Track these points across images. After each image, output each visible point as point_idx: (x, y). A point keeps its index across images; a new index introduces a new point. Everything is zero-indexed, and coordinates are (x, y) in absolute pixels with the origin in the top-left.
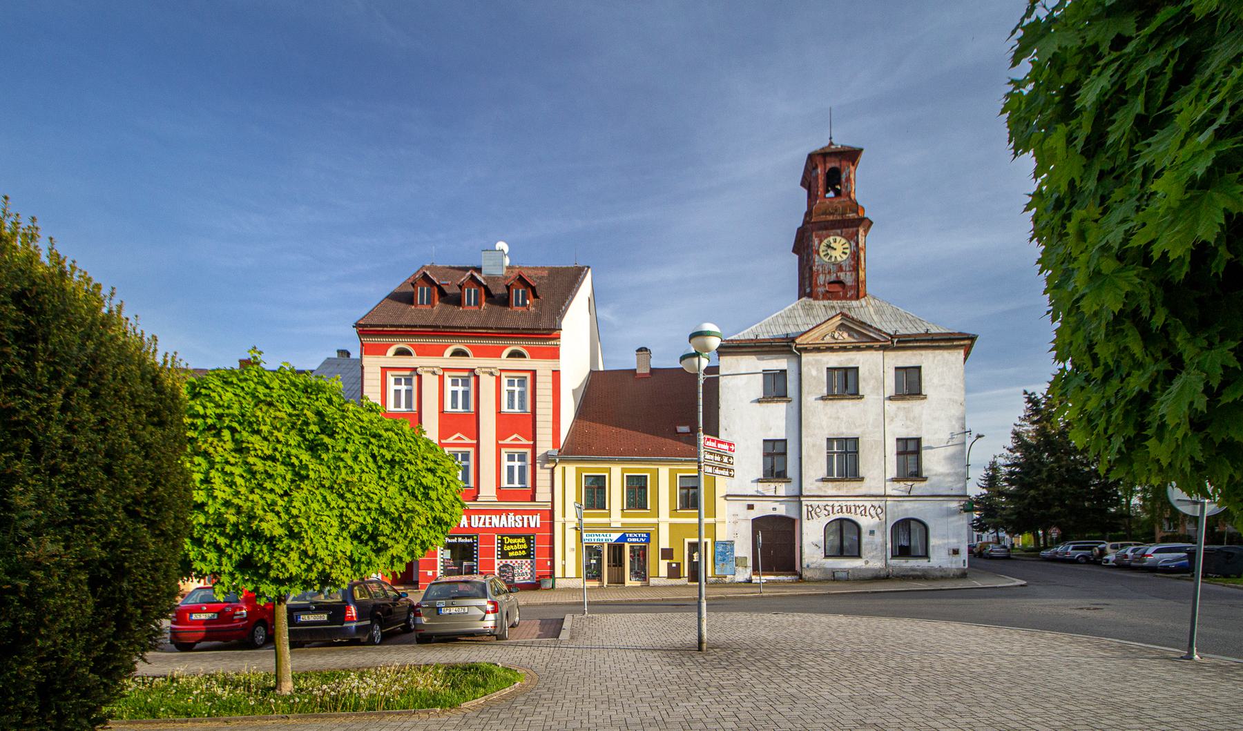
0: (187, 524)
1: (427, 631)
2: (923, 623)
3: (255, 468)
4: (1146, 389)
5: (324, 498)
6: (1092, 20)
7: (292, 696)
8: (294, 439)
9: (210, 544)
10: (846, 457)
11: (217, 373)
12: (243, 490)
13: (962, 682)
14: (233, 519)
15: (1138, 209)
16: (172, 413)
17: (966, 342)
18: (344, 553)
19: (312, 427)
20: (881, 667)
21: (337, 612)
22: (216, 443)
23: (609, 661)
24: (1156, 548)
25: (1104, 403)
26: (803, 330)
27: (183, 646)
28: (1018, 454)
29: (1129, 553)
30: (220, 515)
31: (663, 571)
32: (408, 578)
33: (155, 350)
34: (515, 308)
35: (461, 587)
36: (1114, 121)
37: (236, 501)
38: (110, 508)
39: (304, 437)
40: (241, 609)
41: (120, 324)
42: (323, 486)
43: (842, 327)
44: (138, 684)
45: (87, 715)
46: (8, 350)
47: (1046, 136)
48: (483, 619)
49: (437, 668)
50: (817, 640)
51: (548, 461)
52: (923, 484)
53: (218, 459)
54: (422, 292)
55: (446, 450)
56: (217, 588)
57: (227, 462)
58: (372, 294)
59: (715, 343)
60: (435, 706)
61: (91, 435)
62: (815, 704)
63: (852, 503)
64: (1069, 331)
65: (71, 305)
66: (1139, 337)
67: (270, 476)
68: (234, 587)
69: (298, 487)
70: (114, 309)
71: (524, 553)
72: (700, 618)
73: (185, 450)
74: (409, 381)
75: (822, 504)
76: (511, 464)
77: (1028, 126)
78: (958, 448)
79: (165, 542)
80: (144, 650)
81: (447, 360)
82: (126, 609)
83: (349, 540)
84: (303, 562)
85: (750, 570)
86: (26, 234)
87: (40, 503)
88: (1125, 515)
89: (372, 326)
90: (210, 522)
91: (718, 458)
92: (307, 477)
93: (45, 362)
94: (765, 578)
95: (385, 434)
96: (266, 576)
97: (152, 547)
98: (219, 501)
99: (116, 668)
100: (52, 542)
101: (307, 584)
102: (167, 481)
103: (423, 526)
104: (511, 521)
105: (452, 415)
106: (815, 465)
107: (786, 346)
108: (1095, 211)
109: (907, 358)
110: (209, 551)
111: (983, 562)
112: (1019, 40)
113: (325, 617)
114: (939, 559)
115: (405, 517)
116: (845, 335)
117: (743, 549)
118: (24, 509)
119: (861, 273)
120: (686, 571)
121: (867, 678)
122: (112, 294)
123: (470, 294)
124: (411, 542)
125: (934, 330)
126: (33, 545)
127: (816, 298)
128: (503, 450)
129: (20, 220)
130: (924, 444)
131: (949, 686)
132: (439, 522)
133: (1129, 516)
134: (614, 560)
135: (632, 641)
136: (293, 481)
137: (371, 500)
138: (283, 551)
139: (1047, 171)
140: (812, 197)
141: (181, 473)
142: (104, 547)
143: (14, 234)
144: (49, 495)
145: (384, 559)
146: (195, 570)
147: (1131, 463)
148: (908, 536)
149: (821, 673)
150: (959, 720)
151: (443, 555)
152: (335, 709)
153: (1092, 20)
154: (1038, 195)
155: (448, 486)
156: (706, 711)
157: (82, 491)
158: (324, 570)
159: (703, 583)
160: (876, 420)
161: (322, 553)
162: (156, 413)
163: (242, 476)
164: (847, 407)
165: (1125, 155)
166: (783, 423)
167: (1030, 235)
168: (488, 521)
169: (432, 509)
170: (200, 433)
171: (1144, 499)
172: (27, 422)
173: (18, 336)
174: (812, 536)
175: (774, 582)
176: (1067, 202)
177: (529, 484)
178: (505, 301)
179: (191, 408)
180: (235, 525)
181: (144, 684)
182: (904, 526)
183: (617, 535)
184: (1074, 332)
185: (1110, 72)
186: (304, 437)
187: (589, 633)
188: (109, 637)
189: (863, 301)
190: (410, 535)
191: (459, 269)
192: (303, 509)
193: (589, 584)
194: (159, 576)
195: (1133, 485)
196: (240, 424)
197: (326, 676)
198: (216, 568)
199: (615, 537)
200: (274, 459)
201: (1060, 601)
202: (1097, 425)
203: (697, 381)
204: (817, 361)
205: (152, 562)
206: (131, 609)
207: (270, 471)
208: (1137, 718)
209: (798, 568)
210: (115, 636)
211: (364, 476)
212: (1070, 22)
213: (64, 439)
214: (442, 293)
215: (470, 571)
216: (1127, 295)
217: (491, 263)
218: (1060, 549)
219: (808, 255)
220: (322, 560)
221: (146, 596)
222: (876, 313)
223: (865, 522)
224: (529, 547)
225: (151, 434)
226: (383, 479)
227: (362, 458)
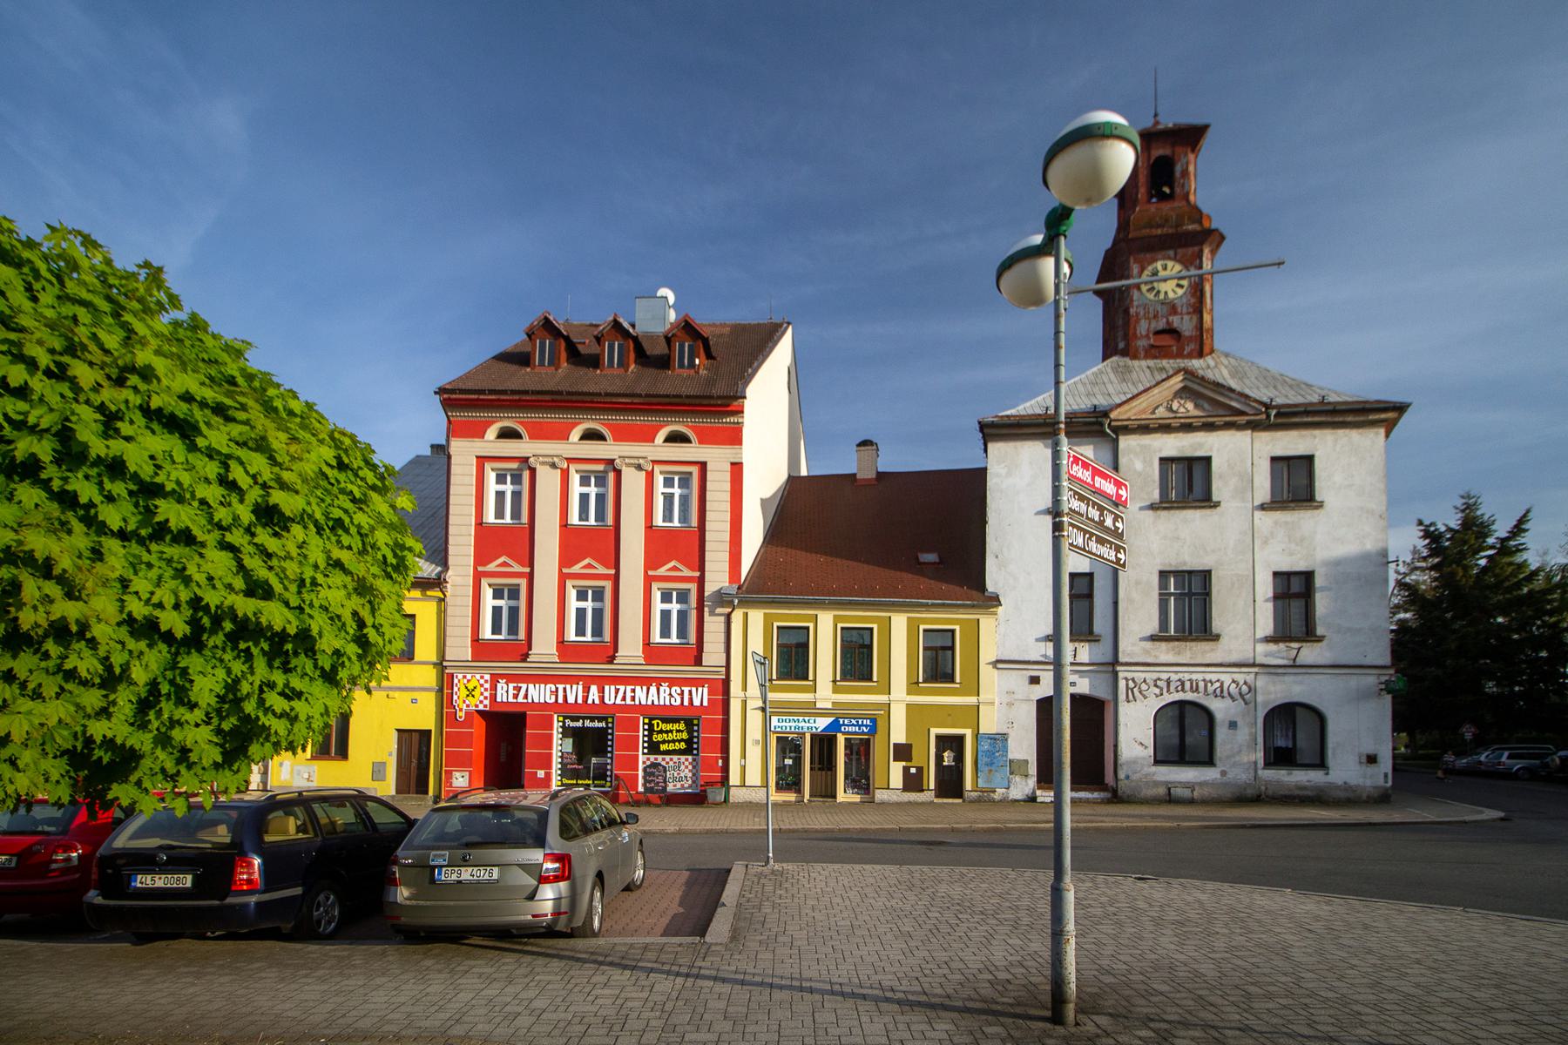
10: (1190, 601)
17: (1390, 415)
21: (215, 869)
26: (1118, 401)
28: (1408, 615)
34: (678, 371)
43: (1184, 392)
51: (722, 603)
63: (1200, 677)
71: (683, 745)
75: (1150, 677)
76: (666, 606)
81: (573, 445)
85: (1032, 782)
91: (1094, 514)
104: (665, 696)
105: (578, 530)
106: (1139, 613)
107: (1095, 425)
109: (1291, 443)
113: (187, 881)
114: (1344, 769)
116: (1190, 406)
117: (1023, 747)
119: (1207, 317)
120: (931, 781)
123: (613, 350)
125: (1333, 398)
127: (1135, 357)
128: (655, 586)
134: (812, 761)
148: (1292, 732)
164: (1192, 521)
168: (629, 694)
174: (1134, 732)
177: (693, 639)
182: (1284, 715)
189: (1209, 360)
199: (822, 723)
204: (1144, 447)
224: (691, 738)
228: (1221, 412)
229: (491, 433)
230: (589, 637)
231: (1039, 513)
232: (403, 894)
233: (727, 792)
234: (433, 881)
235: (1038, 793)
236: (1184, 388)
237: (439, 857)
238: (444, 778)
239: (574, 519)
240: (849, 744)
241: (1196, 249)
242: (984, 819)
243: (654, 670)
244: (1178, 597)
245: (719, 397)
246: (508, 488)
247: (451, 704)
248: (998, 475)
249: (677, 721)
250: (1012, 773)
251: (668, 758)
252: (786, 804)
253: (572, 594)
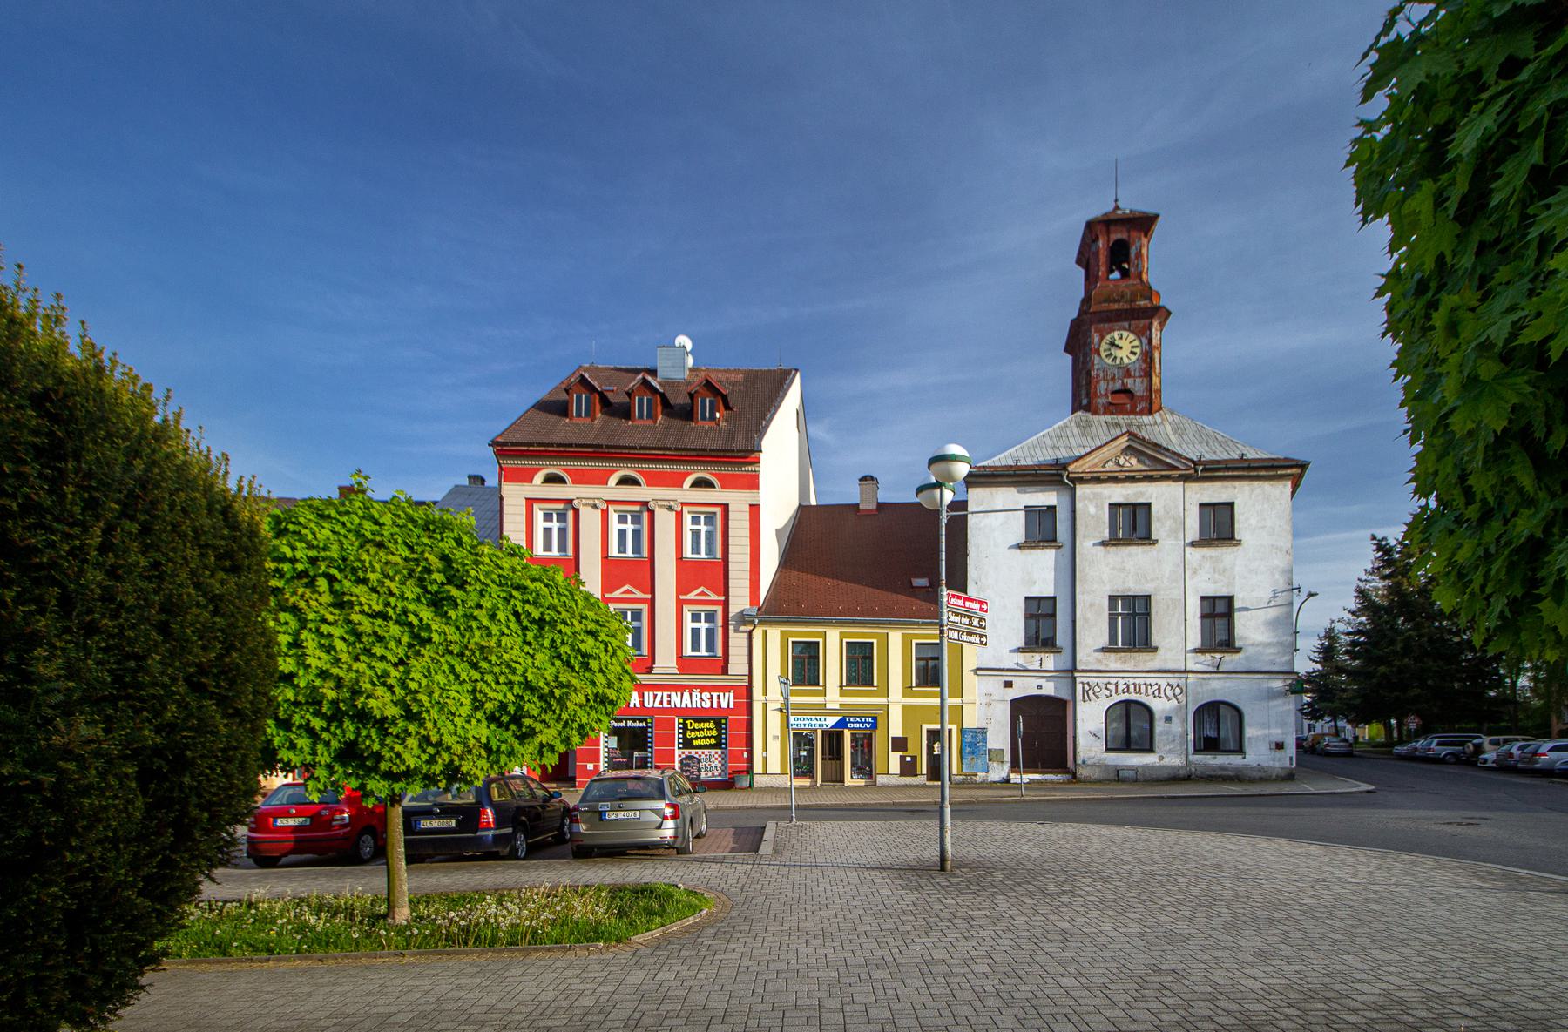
0: (271, 700)
1: (587, 842)
2: (1236, 838)
3: (360, 628)
4: (1539, 534)
5: (452, 668)
6: (1473, 37)
7: (408, 927)
8: (412, 591)
9: (300, 726)
10: (1134, 621)
11: (309, 504)
12: (344, 657)
13: (1289, 917)
14: (331, 694)
15: (1531, 293)
16: (249, 556)
17: (1294, 471)
18: (478, 740)
19: (435, 576)
20: (1180, 896)
21: (468, 816)
22: (308, 595)
23: (824, 883)
24: (1552, 744)
25: (1480, 552)
27: (264, 859)
28: (1363, 619)
29: (1515, 751)
30: (315, 689)
32: (562, 773)
33: (227, 473)
34: (701, 423)
35: (631, 785)
36: (1499, 176)
37: (335, 671)
38: (166, 679)
39: (424, 588)
40: (343, 812)
41: (179, 437)
42: (451, 653)
43: (1129, 450)
44: (204, 911)
45: (133, 953)
46: (27, 469)
47: (1406, 196)
48: (660, 827)
49: (600, 890)
50: (1096, 859)
51: (745, 623)
52: (1236, 657)
53: (311, 616)
54: (579, 401)
55: (612, 607)
56: (311, 784)
57: (324, 621)
58: (515, 403)
59: (962, 470)
60: (597, 939)
61: (141, 584)
62: (1094, 942)
63: (1141, 681)
64: (1433, 457)
65: (112, 411)
66: (1529, 464)
67: (380, 639)
68: (333, 783)
69: (418, 653)
70: (171, 417)
71: (713, 741)
72: (942, 829)
73: (267, 604)
74: (562, 517)
77: (1382, 182)
78: (1283, 610)
79: (240, 724)
80: (212, 866)
81: (612, 490)
82: (187, 813)
83: (485, 723)
84: (424, 751)
85: (1007, 766)
86: (47, 317)
87: (72, 672)
88: (1510, 701)
89: (513, 444)
90: (301, 698)
91: (966, 621)
92: (430, 640)
93: (77, 486)
94: (1027, 777)
95: (531, 586)
96: (375, 769)
97: (224, 731)
98: (313, 671)
99: (173, 890)
100: (87, 723)
101: (430, 779)
102: (243, 644)
103: (581, 706)
104: (696, 700)
106: (1093, 630)
107: (1054, 475)
108: (1472, 297)
109: (1215, 492)
110: (299, 736)
111: (1316, 759)
112: (1372, 66)
113: (452, 823)
115: (557, 693)
116: (1134, 461)
117: (999, 738)
118: (50, 680)
119: (1155, 380)
121: (1162, 910)
122: (168, 398)
123: (642, 404)
124: (566, 725)
126: (62, 727)
127: (1095, 413)
128: (686, 608)
129: (39, 296)
130: (1237, 605)
131: (1272, 922)
132: (603, 700)
133: (1516, 702)
134: (828, 752)
135: (854, 857)
136: (410, 646)
137: (514, 671)
138: (397, 736)
139: (1407, 243)
140: (1090, 279)
141: (263, 634)
142: (158, 730)
143: (31, 316)
144: (84, 661)
145: (531, 748)
146: (281, 760)
147: (1517, 633)
148: (1216, 725)
149: (1102, 901)
150: (1285, 968)
151: (607, 743)
152: (466, 944)
153: (1473, 37)
154: (1394, 276)
155: (614, 654)
156: (951, 950)
157: (128, 657)
158: (452, 761)
159: (947, 783)
160: (1174, 573)
161: (449, 740)
162: (229, 555)
163: (343, 639)
164: (1136, 555)
165: (1514, 219)
166: (1052, 575)
167: (1382, 329)
169: (593, 683)
170: (288, 582)
171: (1535, 679)
172: (54, 564)
173: (39, 452)
174: (1089, 723)
175: (1038, 782)
176: (1433, 285)
177: (719, 652)
178: (687, 414)
179: (275, 548)
180: (334, 703)
181: (211, 910)
182: (1210, 712)
183: (835, 719)
184: (1440, 458)
185: (1497, 108)
186: (424, 588)
187: (798, 846)
188: (164, 848)
189: (1157, 416)
190: (565, 716)
191: (627, 371)
192: (424, 682)
193: (798, 782)
194: (232, 768)
195: (1520, 660)
196: (341, 570)
197: (455, 900)
198: (309, 758)
199: (831, 721)
200: (385, 617)
201: (1422, 813)
202: (1471, 582)
203: (938, 521)
204: (1096, 495)
205: (224, 750)
206: (194, 812)
207: (380, 632)
208: (1528, 971)
209: (1070, 764)
210: (173, 848)
211: (504, 640)
212: (1443, 41)
213: (104, 589)
214: (605, 402)
215: (643, 764)
216: (1514, 408)
217: (669, 363)
218: (1421, 743)
219: (1085, 355)
220: (448, 749)
221: (215, 794)
222: (1175, 431)
223: (1159, 705)
225: (222, 582)
226: (529, 644)
227: (501, 616)
229: (539, 478)
237: (604, 806)
240: (854, 738)
243: (687, 679)
249: (707, 721)
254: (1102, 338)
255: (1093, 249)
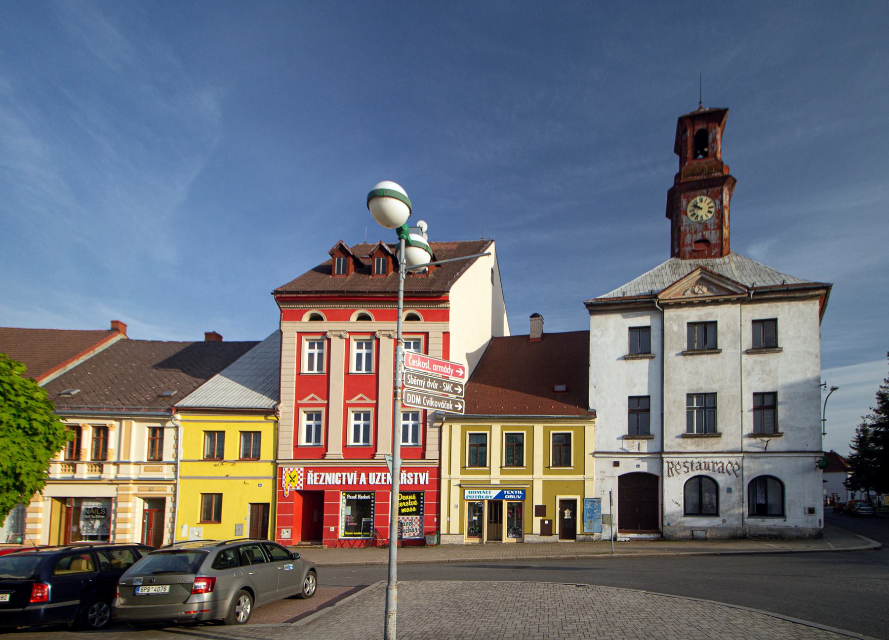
10: (704, 411)
28: (883, 415)
31: (537, 528)
43: (702, 281)
63: (710, 460)
71: (414, 509)
75: (682, 460)
76: (406, 422)
81: (353, 323)
85: (616, 528)
106: (675, 421)
107: (648, 303)
109: (763, 311)
114: (796, 517)
116: (705, 289)
117: (611, 508)
119: (725, 231)
125: (790, 281)
127: (683, 258)
134: (488, 517)
140: (682, 163)
148: (765, 494)
174: (673, 496)
177: (420, 443)
189: (726, 259)
199: (494, 493)
204: (678, 316)
222: (737, 268)
228: (723, 293)
230: (361, 443)
231: (618, 359)
232: (119, 602)
233: (439, 539)
234: (134, 594)
235: (619, 535)
236: (701, 278)
238: (277, 533)
239: (305, 370)
240: (510, 506)
241: (719, 188)
242: (585, 551)
244: (699, 410)
245: (434, 292)
246: (364, 351)
247: (281, 487)
248: (596, 336)
250: (603, 523)
251: (406, 517)
252: (473, 545)
253: (351, 416)
254: (688, 202)
255: (684, 138)
